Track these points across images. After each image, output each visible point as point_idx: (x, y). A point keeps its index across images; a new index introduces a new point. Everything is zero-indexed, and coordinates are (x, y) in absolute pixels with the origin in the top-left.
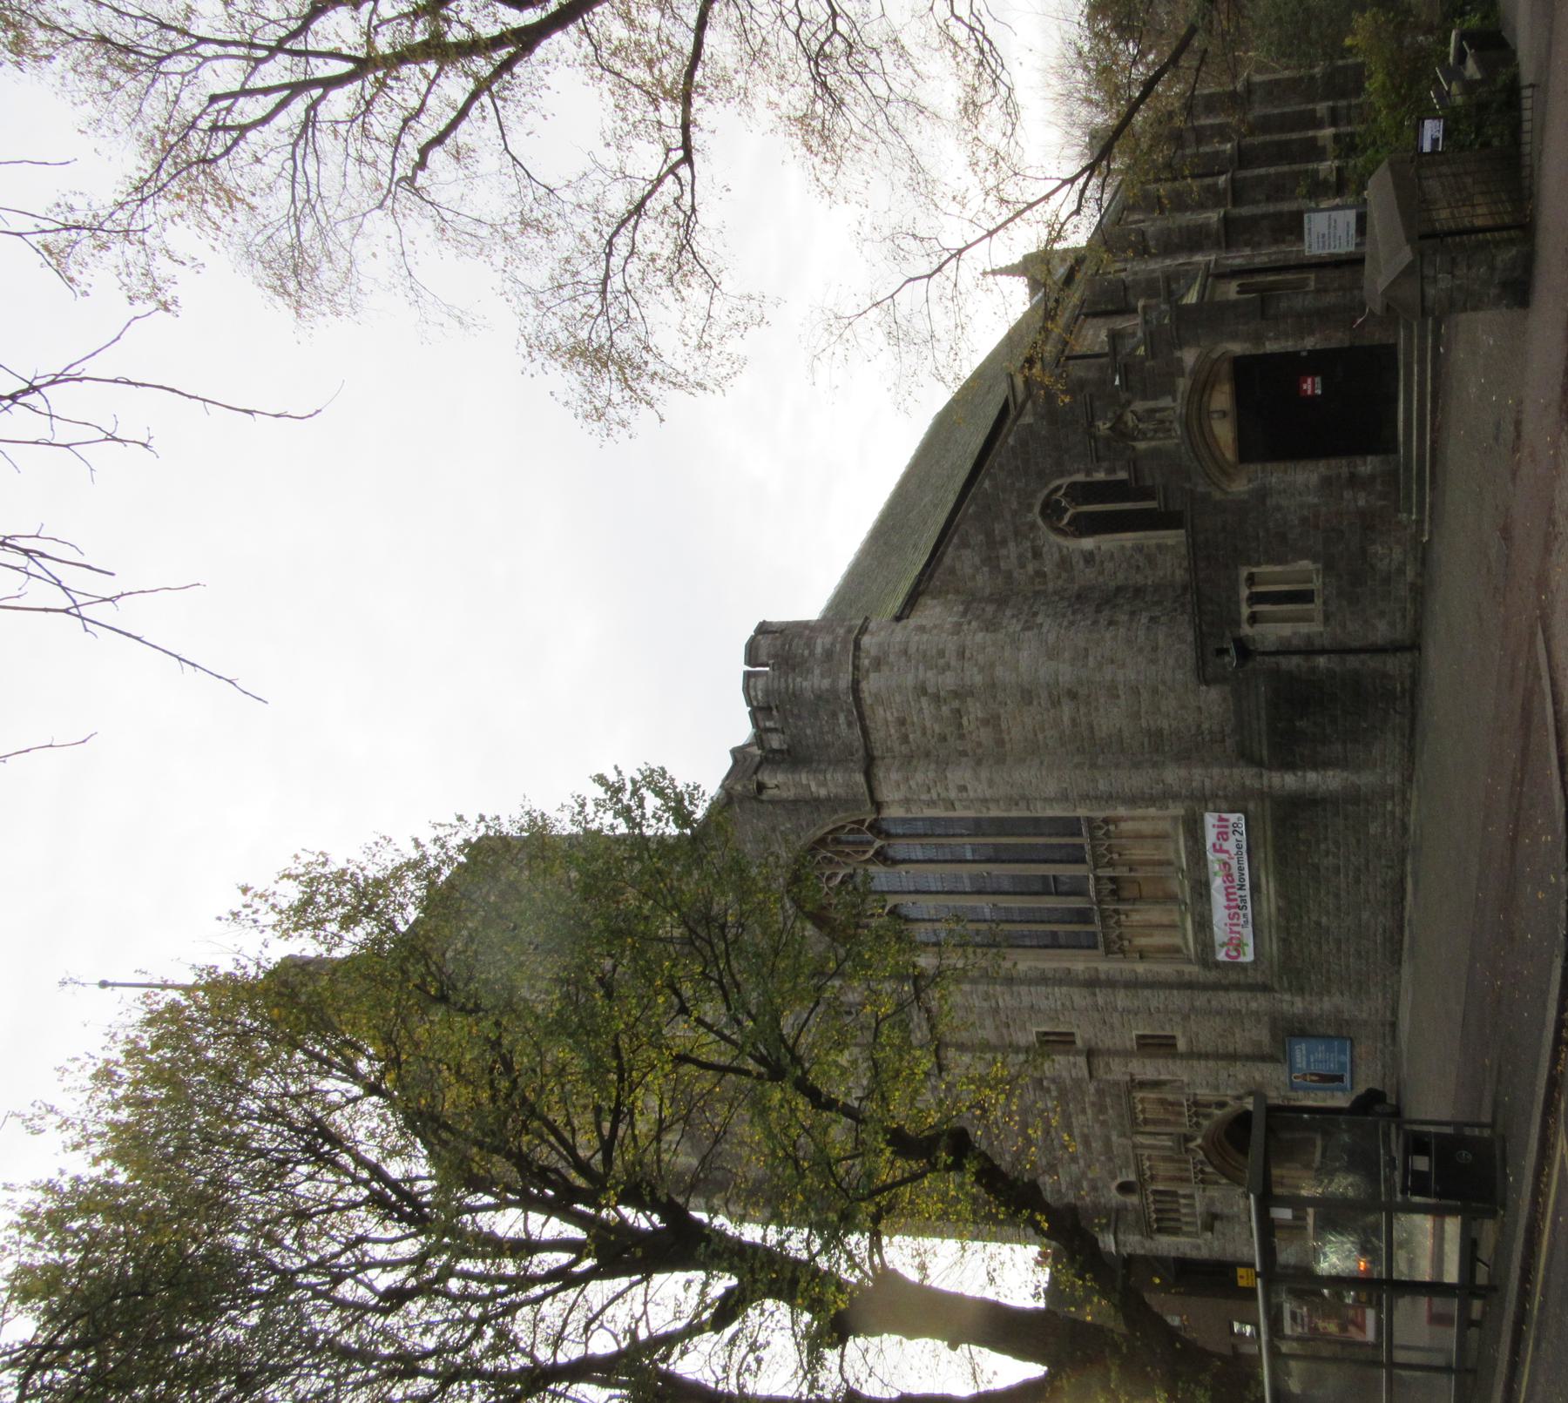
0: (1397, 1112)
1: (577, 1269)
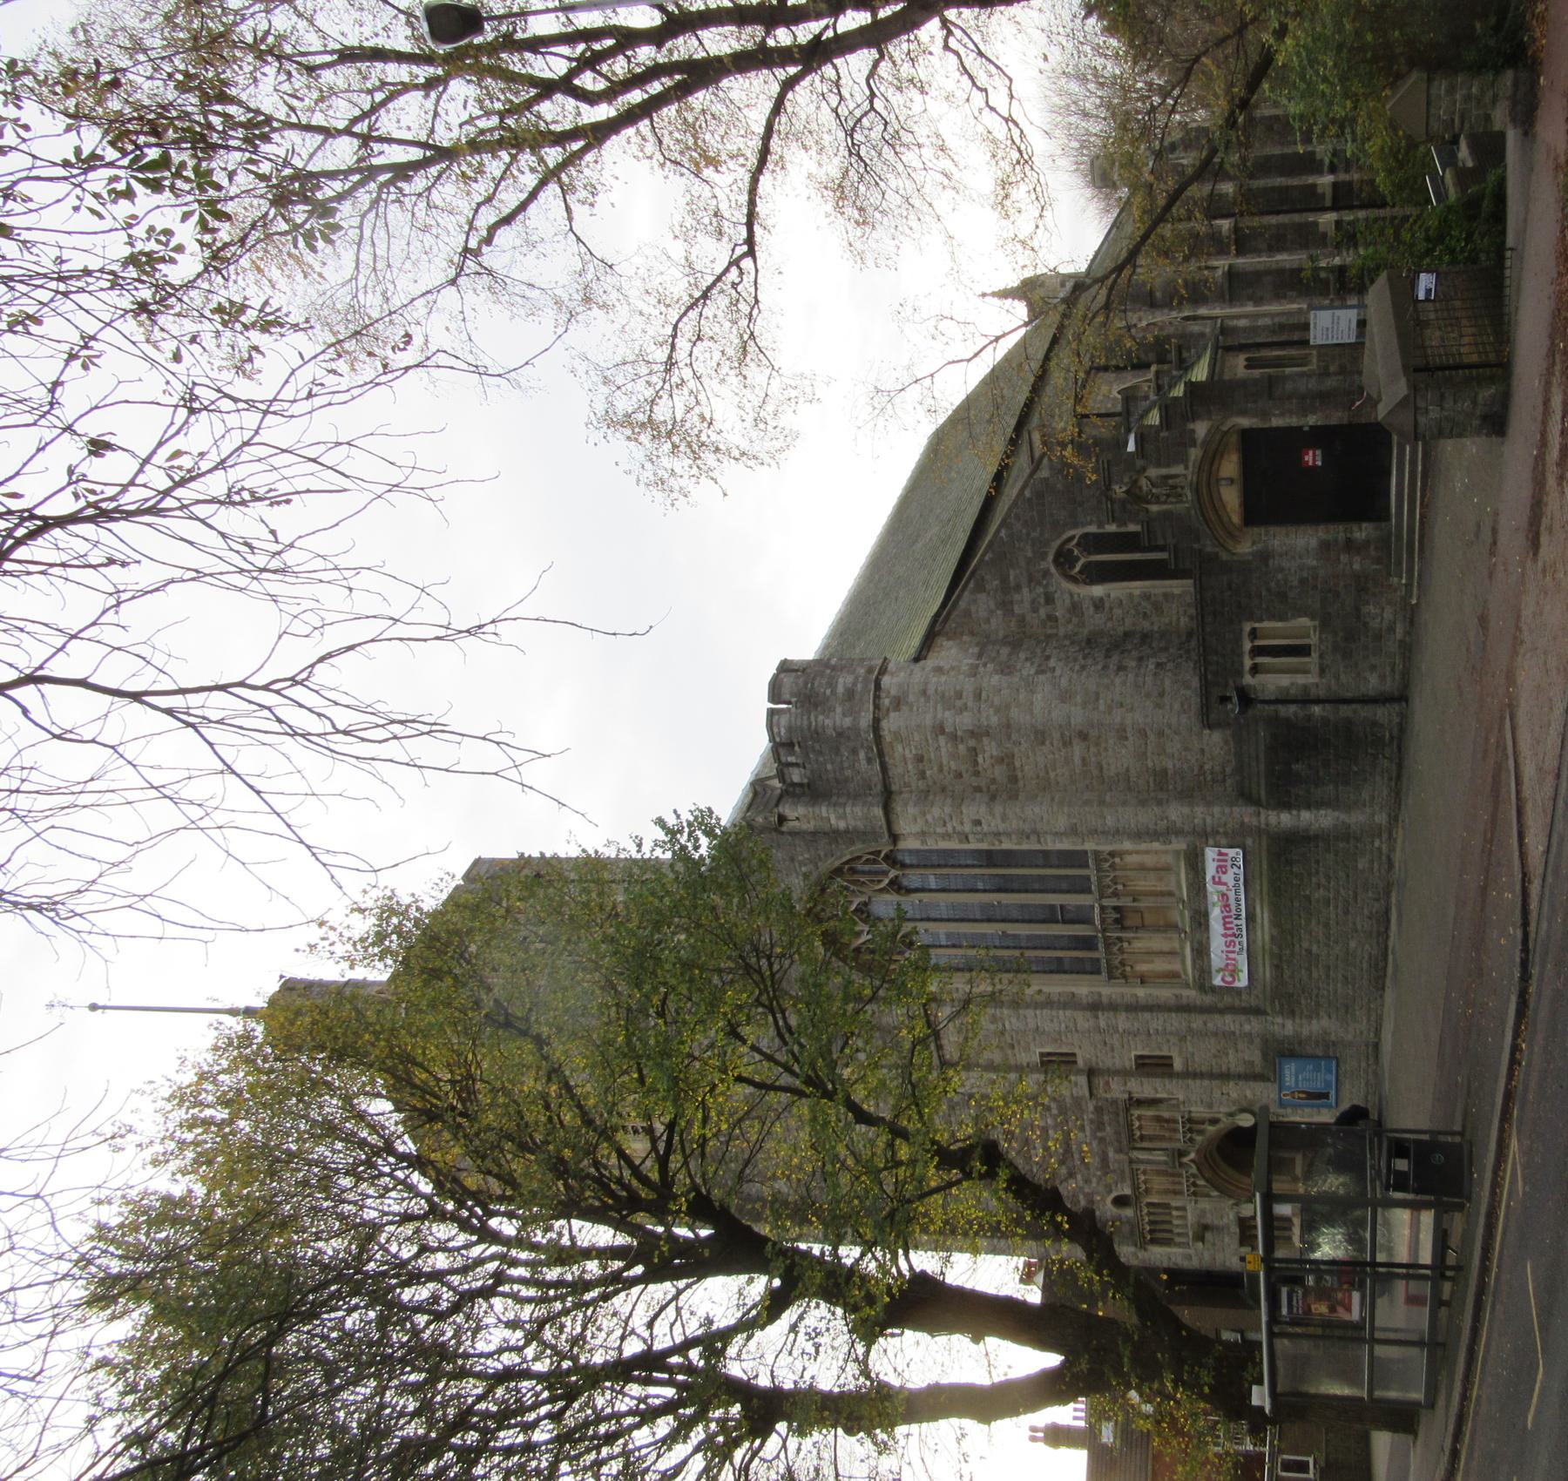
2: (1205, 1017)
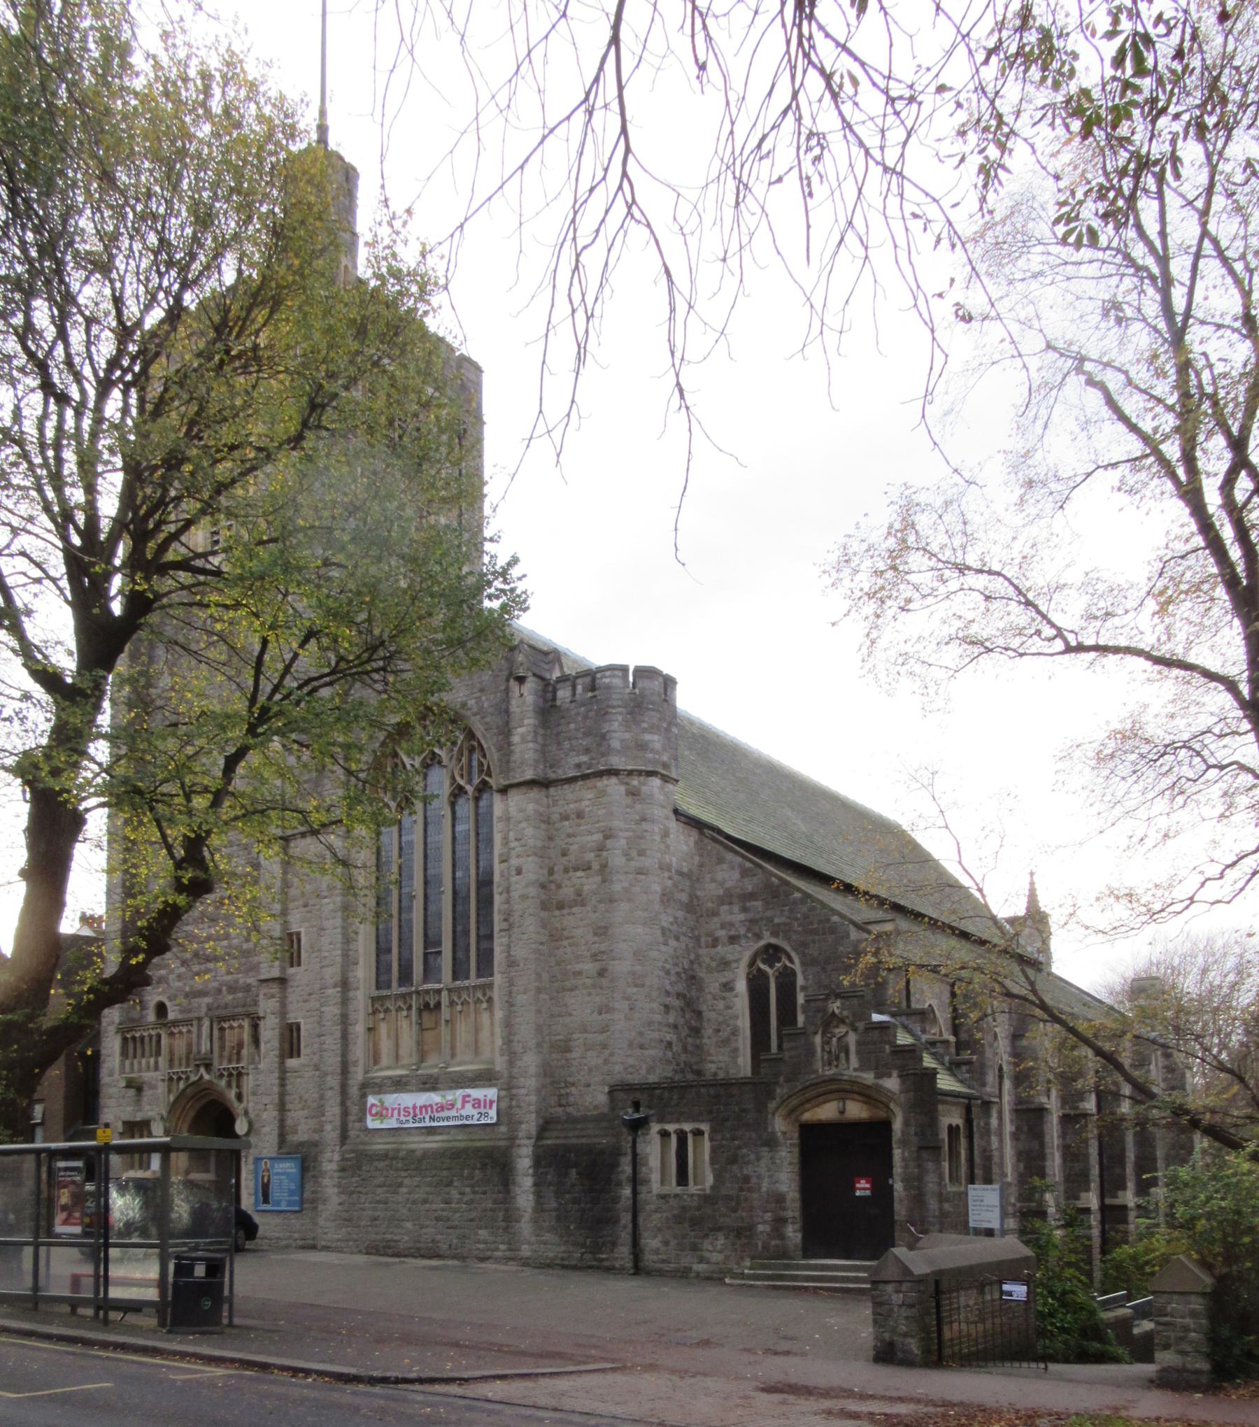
0: (239, 1249)
1: (72, 531)
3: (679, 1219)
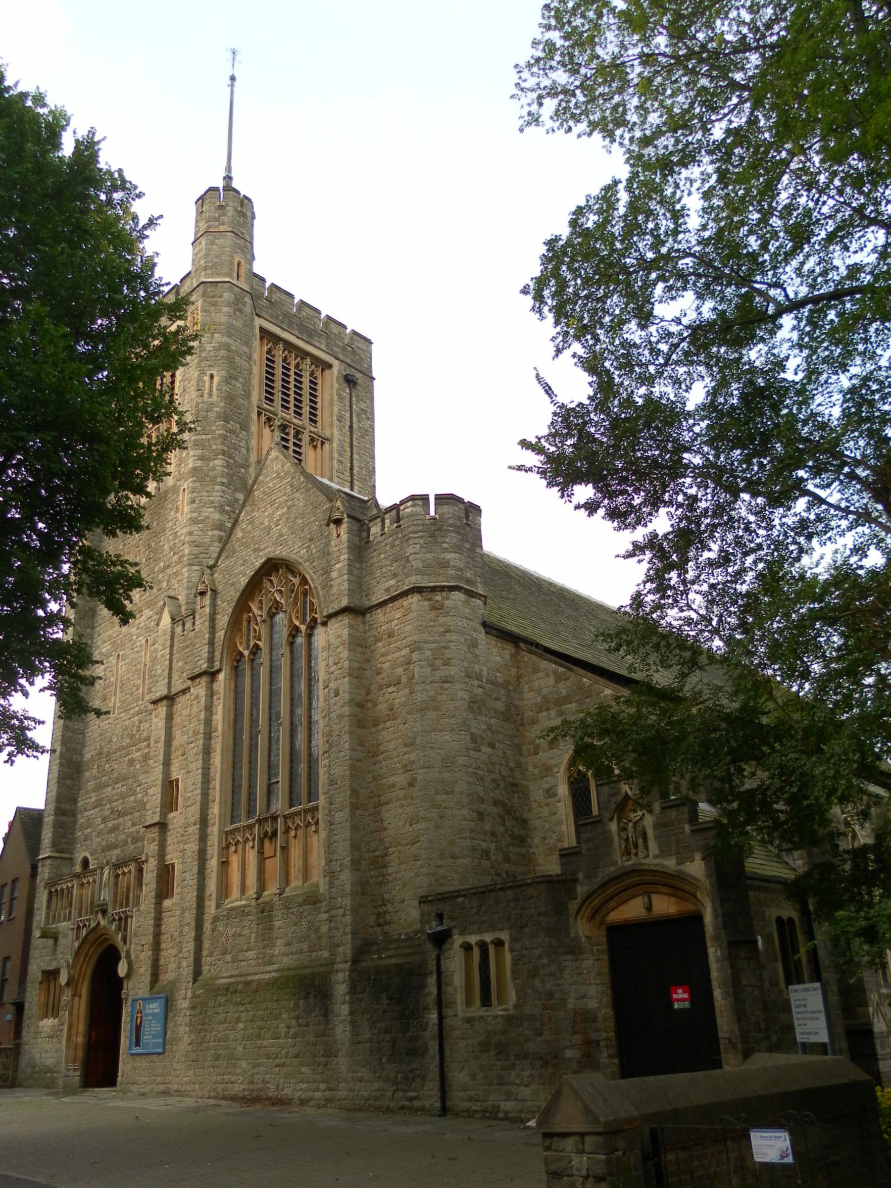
2: (193, 924)
3: (484, 1047)
